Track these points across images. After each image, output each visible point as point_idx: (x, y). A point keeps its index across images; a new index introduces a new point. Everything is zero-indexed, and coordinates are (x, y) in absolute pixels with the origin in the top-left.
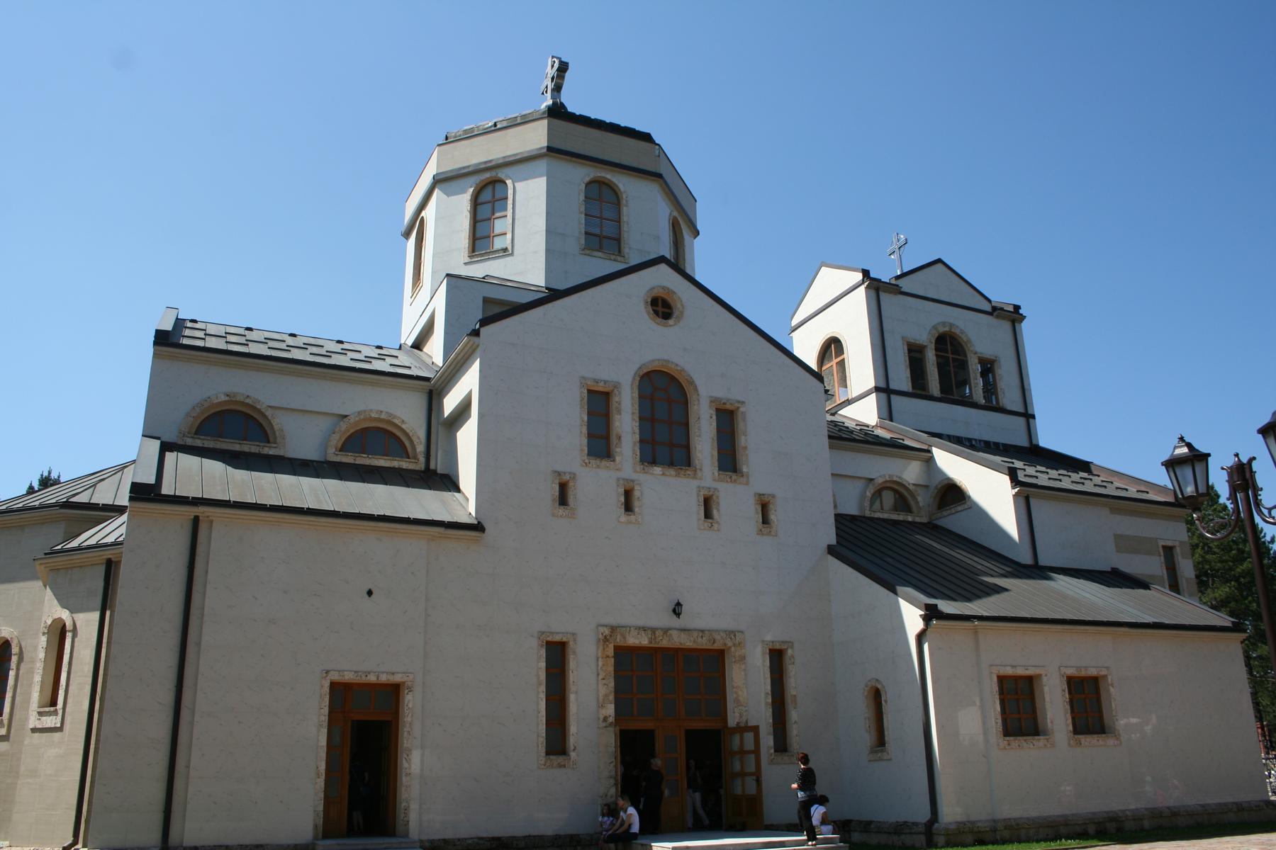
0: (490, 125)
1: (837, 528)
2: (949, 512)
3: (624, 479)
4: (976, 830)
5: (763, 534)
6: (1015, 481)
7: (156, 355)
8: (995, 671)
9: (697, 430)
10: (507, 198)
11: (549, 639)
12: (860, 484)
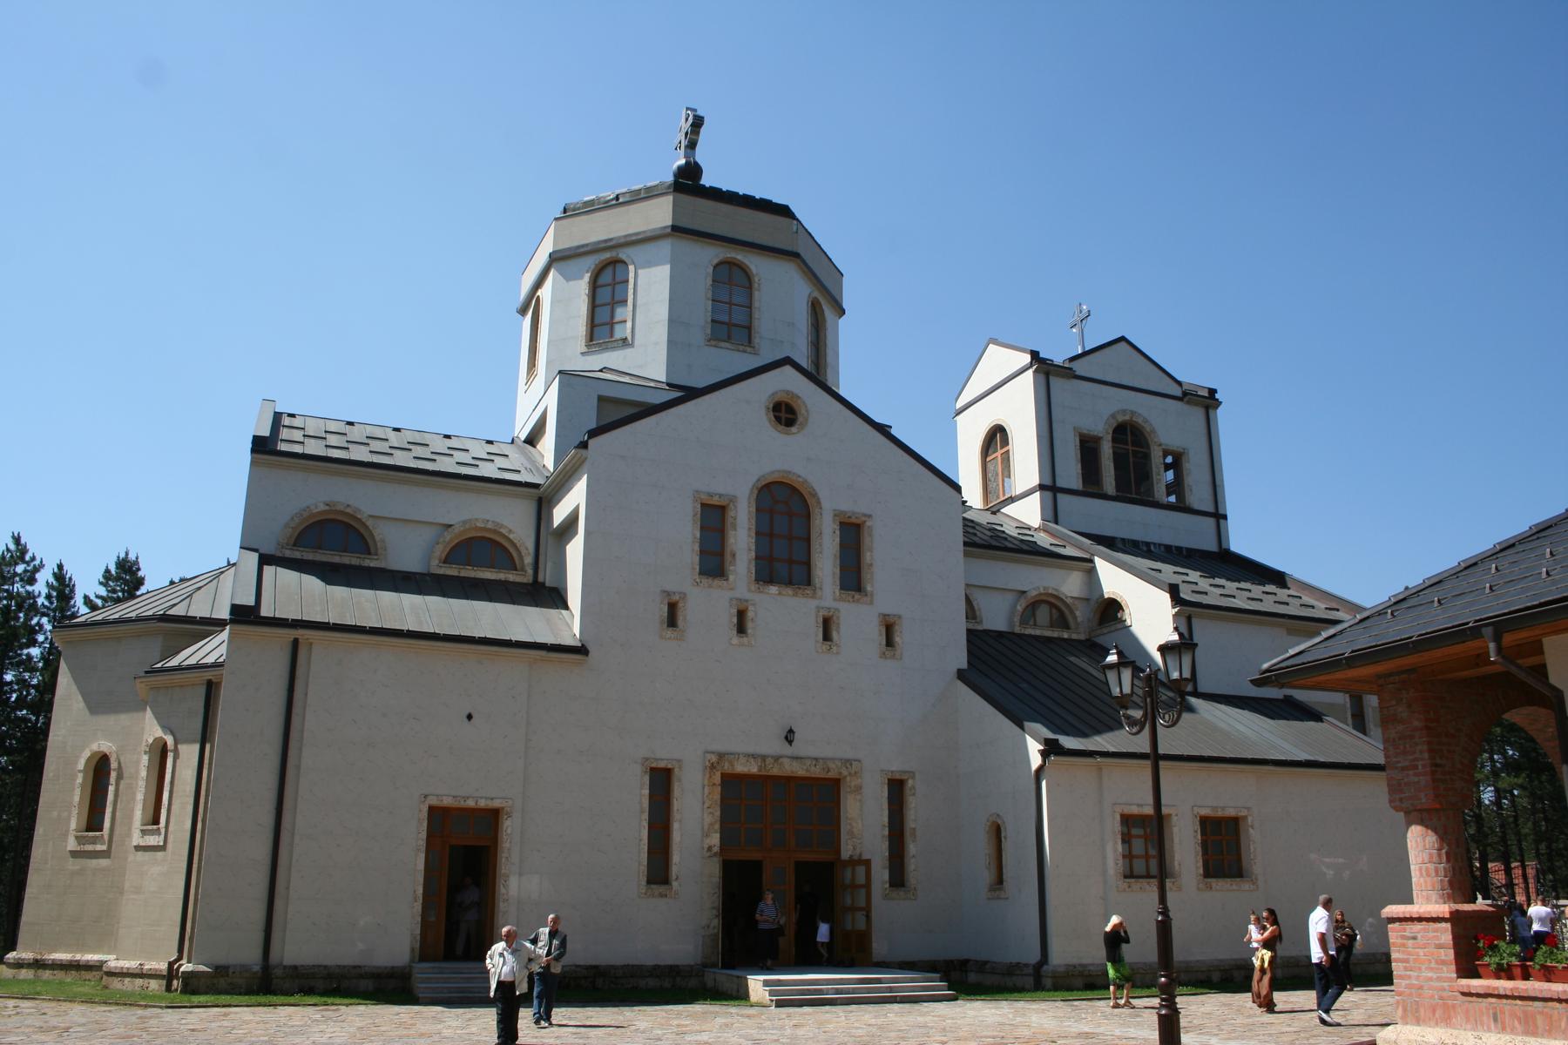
0: (611, 197)
1: (969, 652)
3: (737, 599)
4: (1086, 973)
5: (886, 658)
6: (1176, 599)
8: (1119, 810)
9: (818, 546)
10: (627, 281)
11: (653, 765)
12: (1010, 597)
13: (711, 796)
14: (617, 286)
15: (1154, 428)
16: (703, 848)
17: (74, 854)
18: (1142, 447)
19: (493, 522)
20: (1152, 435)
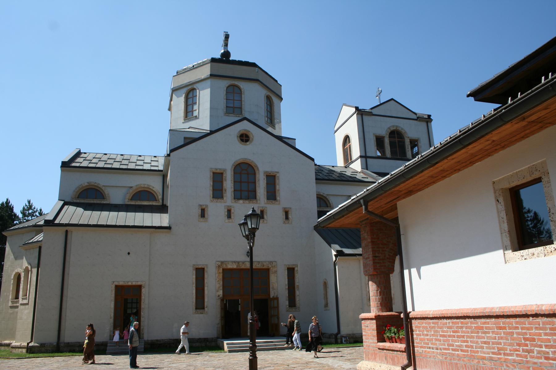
0: (192, 66)
3: (227, 206)
4: (354, 337)
5: (286, 224)
7: (62, 171)
13: (218, 277)
14: (194, 98)
15: (406, 132)
16: (216, 296)
17: (11, 307)
18: (402, 139)
19: (147, 184)
20: (405, 134)
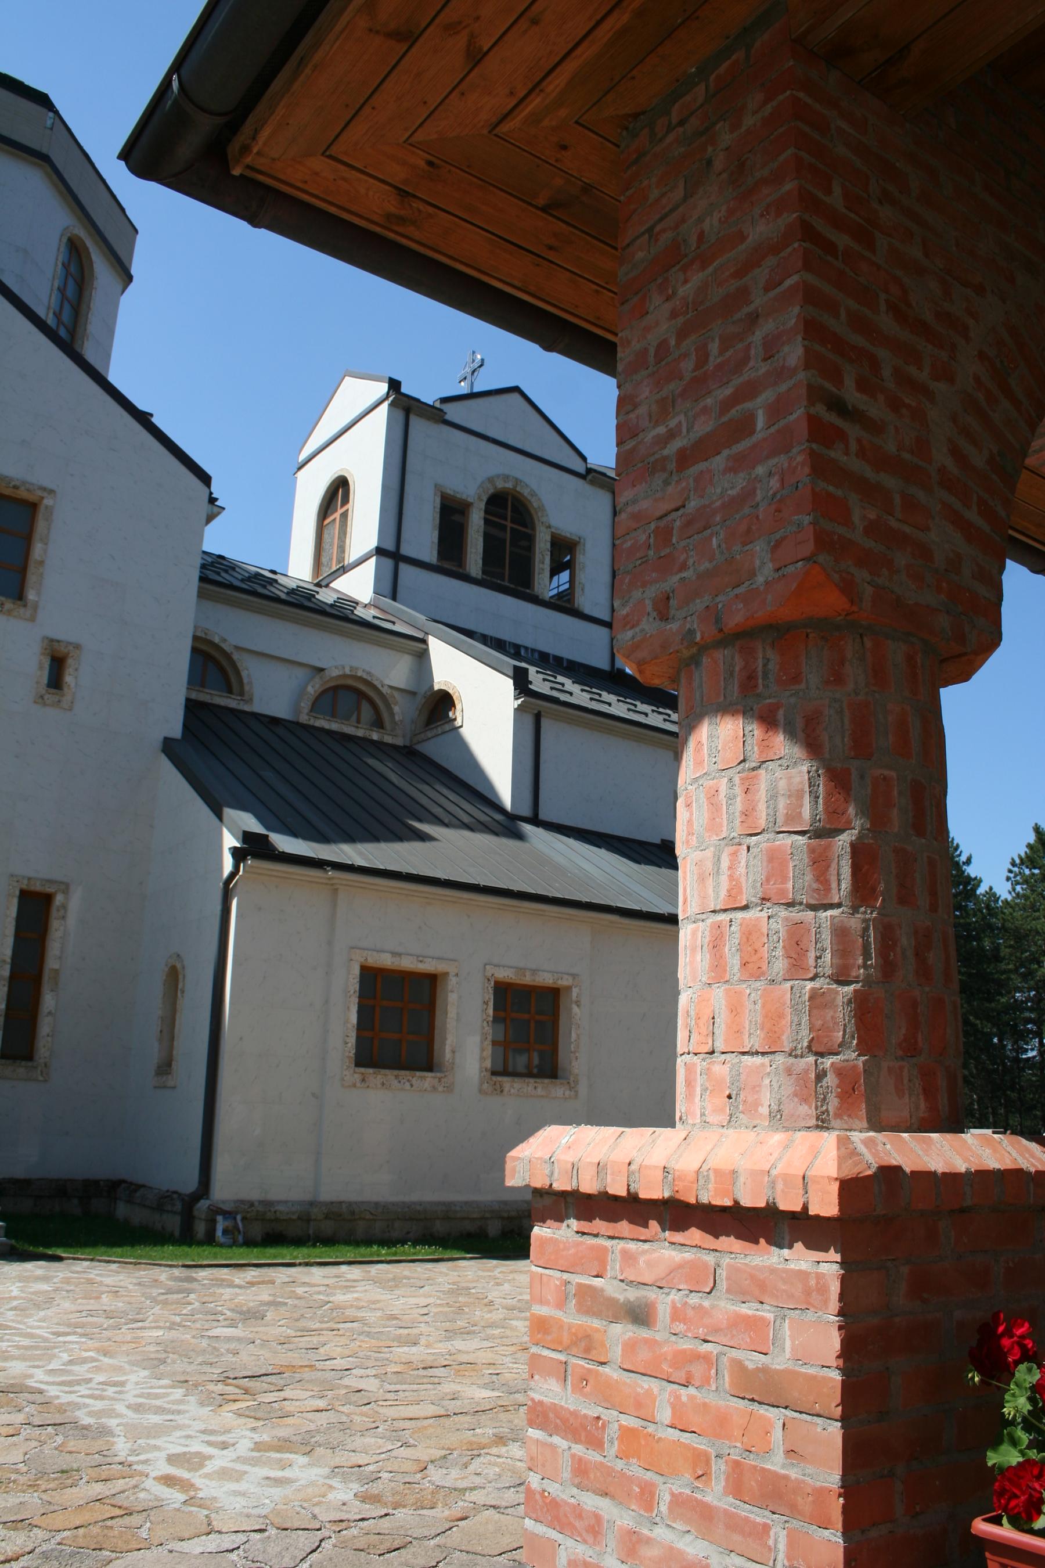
2: (434, 732)
5: (45, 704)
8: (359, 958)
15: (543, 505)
18: (526, 526)
20: (540, 514)
